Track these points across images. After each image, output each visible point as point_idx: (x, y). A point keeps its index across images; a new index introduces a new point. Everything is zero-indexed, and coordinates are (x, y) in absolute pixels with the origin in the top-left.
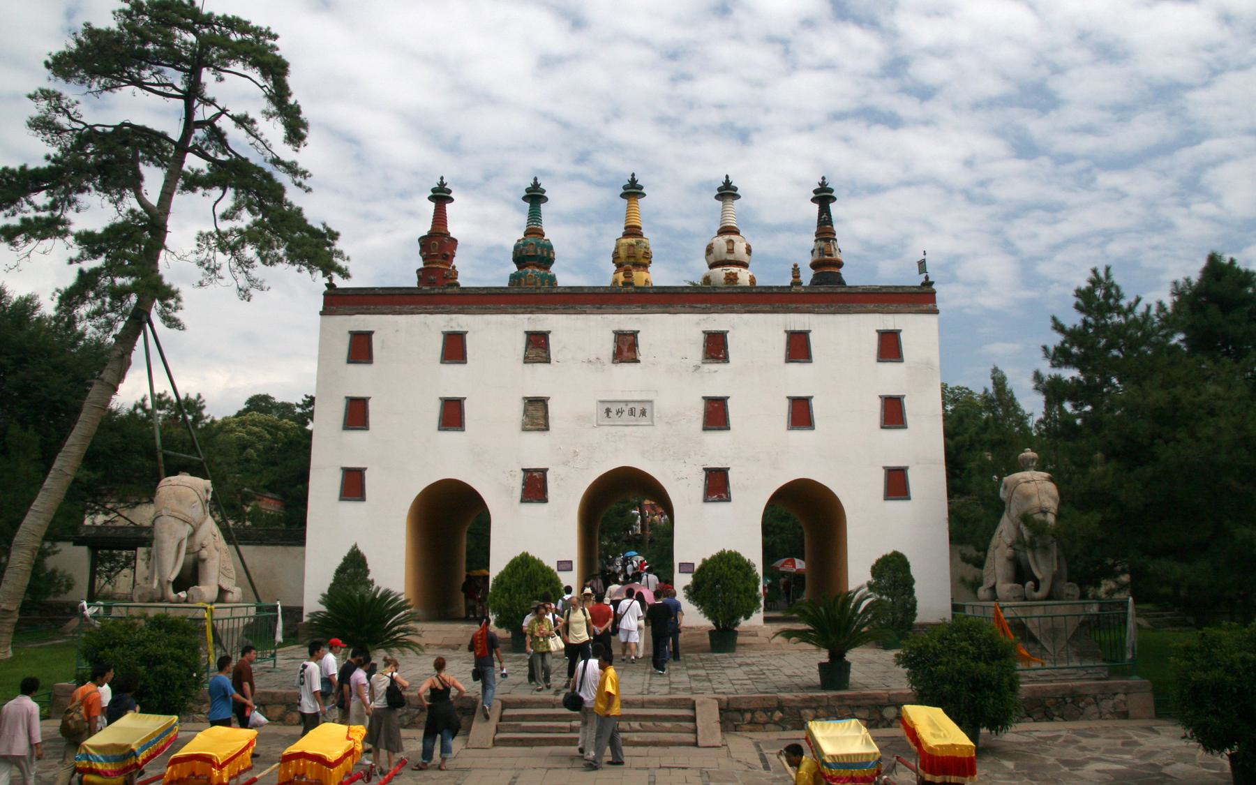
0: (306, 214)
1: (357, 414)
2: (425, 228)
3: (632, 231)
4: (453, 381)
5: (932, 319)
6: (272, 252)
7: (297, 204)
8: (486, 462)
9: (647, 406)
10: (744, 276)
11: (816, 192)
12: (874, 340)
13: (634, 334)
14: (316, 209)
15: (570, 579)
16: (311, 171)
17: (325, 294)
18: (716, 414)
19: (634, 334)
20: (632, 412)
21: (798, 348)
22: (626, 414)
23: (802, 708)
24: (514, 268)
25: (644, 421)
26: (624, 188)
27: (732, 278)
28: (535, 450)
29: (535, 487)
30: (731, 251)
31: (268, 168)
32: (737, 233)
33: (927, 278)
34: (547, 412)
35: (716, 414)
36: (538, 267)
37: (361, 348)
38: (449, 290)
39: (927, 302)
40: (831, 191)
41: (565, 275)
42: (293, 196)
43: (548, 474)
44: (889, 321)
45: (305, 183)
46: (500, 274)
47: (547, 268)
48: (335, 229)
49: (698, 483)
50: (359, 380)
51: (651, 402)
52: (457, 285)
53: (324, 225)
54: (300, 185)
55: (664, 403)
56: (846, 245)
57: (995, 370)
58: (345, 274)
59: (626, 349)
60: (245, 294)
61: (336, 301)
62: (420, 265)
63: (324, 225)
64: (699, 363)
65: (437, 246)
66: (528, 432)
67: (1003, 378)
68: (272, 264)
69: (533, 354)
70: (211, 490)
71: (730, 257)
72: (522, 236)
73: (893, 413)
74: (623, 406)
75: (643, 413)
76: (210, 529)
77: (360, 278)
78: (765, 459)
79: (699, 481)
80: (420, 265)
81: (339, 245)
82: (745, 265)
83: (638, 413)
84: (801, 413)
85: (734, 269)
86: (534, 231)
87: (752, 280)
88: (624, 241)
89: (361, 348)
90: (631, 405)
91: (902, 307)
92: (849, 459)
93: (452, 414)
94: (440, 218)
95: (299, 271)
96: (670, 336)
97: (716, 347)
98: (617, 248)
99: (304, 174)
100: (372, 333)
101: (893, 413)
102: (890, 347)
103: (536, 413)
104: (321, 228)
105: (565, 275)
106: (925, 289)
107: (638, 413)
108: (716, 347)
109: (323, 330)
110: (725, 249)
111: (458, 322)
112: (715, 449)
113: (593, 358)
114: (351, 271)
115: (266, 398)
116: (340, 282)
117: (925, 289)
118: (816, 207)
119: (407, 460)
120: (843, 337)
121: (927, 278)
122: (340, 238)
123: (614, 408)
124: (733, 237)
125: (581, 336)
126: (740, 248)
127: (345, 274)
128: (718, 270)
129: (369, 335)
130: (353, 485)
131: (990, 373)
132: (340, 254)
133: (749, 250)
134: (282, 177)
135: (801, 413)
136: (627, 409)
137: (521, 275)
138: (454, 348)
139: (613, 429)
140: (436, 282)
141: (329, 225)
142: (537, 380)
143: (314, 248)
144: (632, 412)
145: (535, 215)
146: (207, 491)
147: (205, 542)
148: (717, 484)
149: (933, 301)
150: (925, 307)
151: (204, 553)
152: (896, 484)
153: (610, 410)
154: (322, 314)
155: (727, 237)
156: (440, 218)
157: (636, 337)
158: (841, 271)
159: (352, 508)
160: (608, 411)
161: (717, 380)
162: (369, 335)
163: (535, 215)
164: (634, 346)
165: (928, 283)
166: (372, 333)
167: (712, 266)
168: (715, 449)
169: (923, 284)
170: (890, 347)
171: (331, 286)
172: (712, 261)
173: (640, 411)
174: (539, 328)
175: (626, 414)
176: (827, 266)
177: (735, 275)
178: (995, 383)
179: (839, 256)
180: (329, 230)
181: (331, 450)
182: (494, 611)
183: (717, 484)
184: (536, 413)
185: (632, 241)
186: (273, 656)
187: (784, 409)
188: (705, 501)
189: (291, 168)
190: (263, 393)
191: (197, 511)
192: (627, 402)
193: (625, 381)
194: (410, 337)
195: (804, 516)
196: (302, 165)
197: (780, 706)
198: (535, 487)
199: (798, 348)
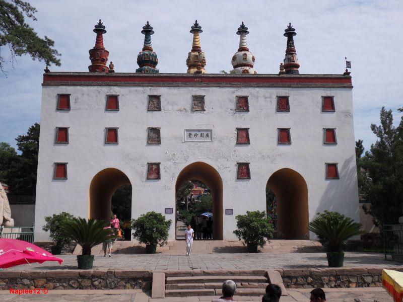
1: (62, 136)
2: (92, 45)
3: (196, 49)
4: (112, 120)
9: (209, 133)
12: (320, 100)
15: (171, 217)
17: (44, 75)
20: (202, 135)
23: (322, 276)
24: (138, 67)
25: (208, 140)
26: (286, 30)
28: (154, 154)
29: (154, 171)
32: (248, 50)
35: (243, 136)
36: (150, 66)
37: (64, 103)
40: (294, 30)
43: (161, 165)
44: (328, 93)
47: (154, 67)
50: (64, 119)
51: (211, 131)
55: (217, 132)
56: (299, 58)
58: (58, 63)
61: (50, 79)
62: (90, 64)
63: (46, 37)
65: (98, 54)
66: (151, 147)
71: (244, 62)
72: (142, 51)
77: (64, 68)
78: (267, 159)
79: (234, 169)
80: (90, 64)
82: (252, 66)
83: (205, 135)
85: (247, 68)
86: (147, 48)
88: (193, 54)
89: (64, 103)
93: (112, 136)
94: (99, 40)
96: (220, 98)
98: (189, 57)
103: (154, 136)
104: (44, 39)
107: (205, 135)
109: (43, 93)
111: (115, 90)
112: (243, 153)
113: (182, 109)
116: (53, 68)
118: (286, 38)
119: (87, 159)
120: (305, 101)
123: (193, 133)
124: (246, 52)
126: (250, 57)
127: (58, 63)
128: (239, 68)
130: (61, 171)
132: (55, 51)
133: (254, 59)
139: (192, 144)
140: (99, 71)
141: (49, 37)
142: (154, 120)
143: (42, 49)
144: (202, 135)
145: (147, 40)
148: (244, 171)
149: (350, 82)
150: (345, 85)
153: (190, 133)
154: (43, 85)
155: (243, 52)
156: (99, 40)
157: (204, 98)
158: (299, 69)
159: (59, 184)
160: (190, 135)
161: (243, 120)
163: (147, 40)
167: (235, 67)
168: (243, 153)
169: (345, 74)
171: (47, 71)
172: (235, 64)
173: (207, 134)
174: (155, 93)
175: (199, 136)
176: (290, 66)
179: (297, 62)
180: (48, 40)
181: (48, 154)
182: (42, 253)
183: (244, 171)
184: (154, 136)
185: (197, 53)
187: (275, 134)
192: (199, 131)
193: (198, 120)
194: (89, 98)
195: (286, 188)
197: (311, 274)
198: (154, 171)
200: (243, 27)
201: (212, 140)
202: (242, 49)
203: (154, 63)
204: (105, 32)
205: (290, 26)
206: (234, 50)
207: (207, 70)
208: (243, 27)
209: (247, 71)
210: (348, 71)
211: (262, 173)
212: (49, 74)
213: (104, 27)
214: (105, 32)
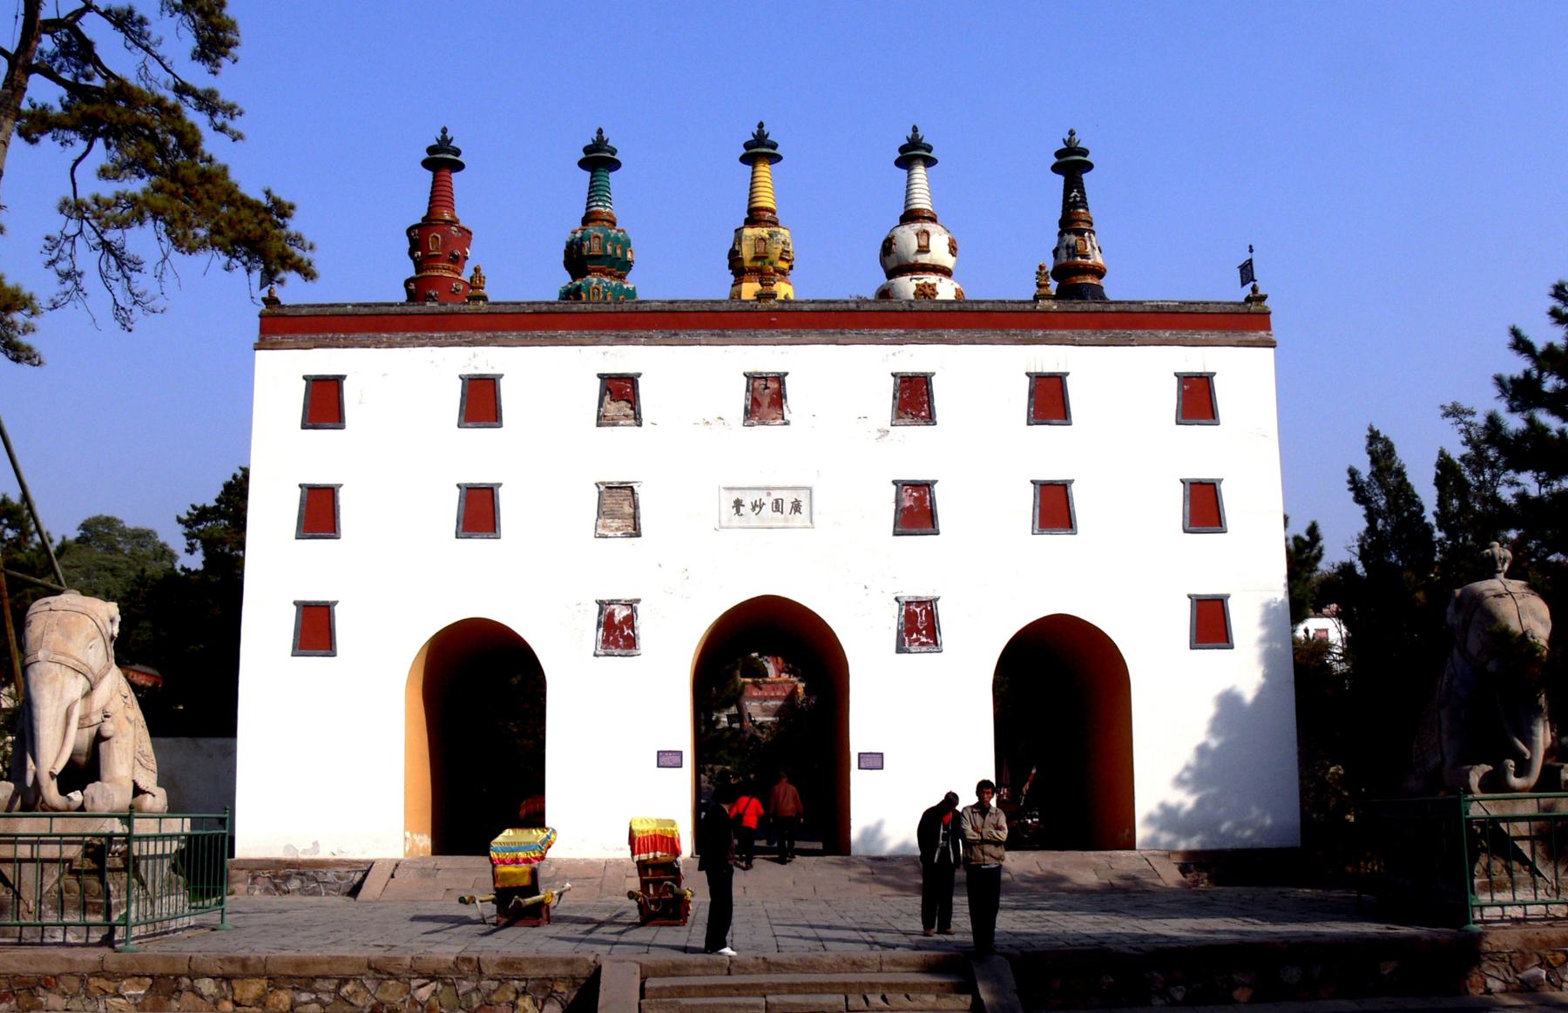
0: (234, 176)
2: (417, 213)
5: (1269, 353)
6: (190, 233)
7: (221, 159)
8: (535, 589)
10: (946, 290)
11: (1059, 154)
13: (780, 378)
14: (247, 166)
16: (241, 106)
18: (917, 511)
19: (780, 378)
20: (778, 506)
21: (1049, 400)
22: (767, 509)
25: (799, 519)
26: (747, 146)
27: (926, 292)
28: (618, 569)
30: (924, 249)
31: (171, 98)
33: (1254, 289)
34: (636, 507)
35: (917, 511)
36: (609, 274)
38: (472, 307)
39: (1255, 329)
40: (1085, 152)
41: (649, 283)
42: (214, 145)
44: (1195, 359)
45: (231, 125)
46: (546, 282)
47: (621, 277)
48: (286, 198)
49: (889, 621)
52: (484, 298)
53: (268, 193)
54: (221, 129)
57: (1374, 437)
59: (766, 398)
60: (122, 317)
63: (268, 193)
64: (887, 426)
67: (1389, 449)
68: (191, 250)
69: (612, 408)
70: (118, 619)
71: (924, 259)
73: (1204, 507)
74: (762, 495)
75: (796, 507)
76: (115, 690)
78: (997, 586)
81: (293, 225)
82: (946, 272)
83: (787, 507)
84: (1055, 507)
85: (931, 279)
87: (959, 293)
88: (748, 232)
90: (776, 495)
91: (1215, 335)
92: (1127, 584)
93: (479, 511)
94: (440, 196)
95: (228, 268)
96: (842, 380)
97: (914, 398)
99: (230, 110)
100: (343, 377)
101: (1204, 507)
102: (1197, 401)
103: (619, 506)
104: (263, 200)
105: (649, 283)
106: (1253, 307)
107: (787, 507)
108: (914, 398)
110: (915, 247)
112: (918, 566)
114: (317, 267)
115: (109, 522)
117: (1253, 307)
118: (1060, 180)
120: (1124, 383)
121: (1254, 289)
122: (295, 214)
123: (748, 501)
124: (929, 226)
125: (692, 380)
129: (336, 382)
130: (315, 629)
131: (1365, 442)
134: (193, 115)
135: (1055, 507)
136: (769, 501)
137: (579, 288)
138: (481, 402)
141: (276, 194)
144: (778, 506)
145: (596, 191)
146: (112, 621)
147: (110, 709)
150: (1252, 336)
151: (108, 729)
152: (1210, 623)
155: (917, 226)
156: (440, 196)
158: (1103, 282)
160: (738, 504)
162: (336, 382)
164: (779, 399)
165: (1257, 298)
166: (343, 377)
167: (891, 274)
169: (1248, 300)
170: (1197, 401)
172: (892, 264)
173: (793, 505)
175: (767, 509)
177: (932, 287)
178: (1374, 461)
180: (277, 203)
185: (763, 232)
186: (221, 903)
188: (900, 649)
189: (208, 102)
190: (107, 513)
191: (97, 654)
193: (767, 454)
196: (225, 96)
199: (1049, 400)
206: (571, 223)
212: (277, 311)
213: (929, 149)
214: (459, 166)
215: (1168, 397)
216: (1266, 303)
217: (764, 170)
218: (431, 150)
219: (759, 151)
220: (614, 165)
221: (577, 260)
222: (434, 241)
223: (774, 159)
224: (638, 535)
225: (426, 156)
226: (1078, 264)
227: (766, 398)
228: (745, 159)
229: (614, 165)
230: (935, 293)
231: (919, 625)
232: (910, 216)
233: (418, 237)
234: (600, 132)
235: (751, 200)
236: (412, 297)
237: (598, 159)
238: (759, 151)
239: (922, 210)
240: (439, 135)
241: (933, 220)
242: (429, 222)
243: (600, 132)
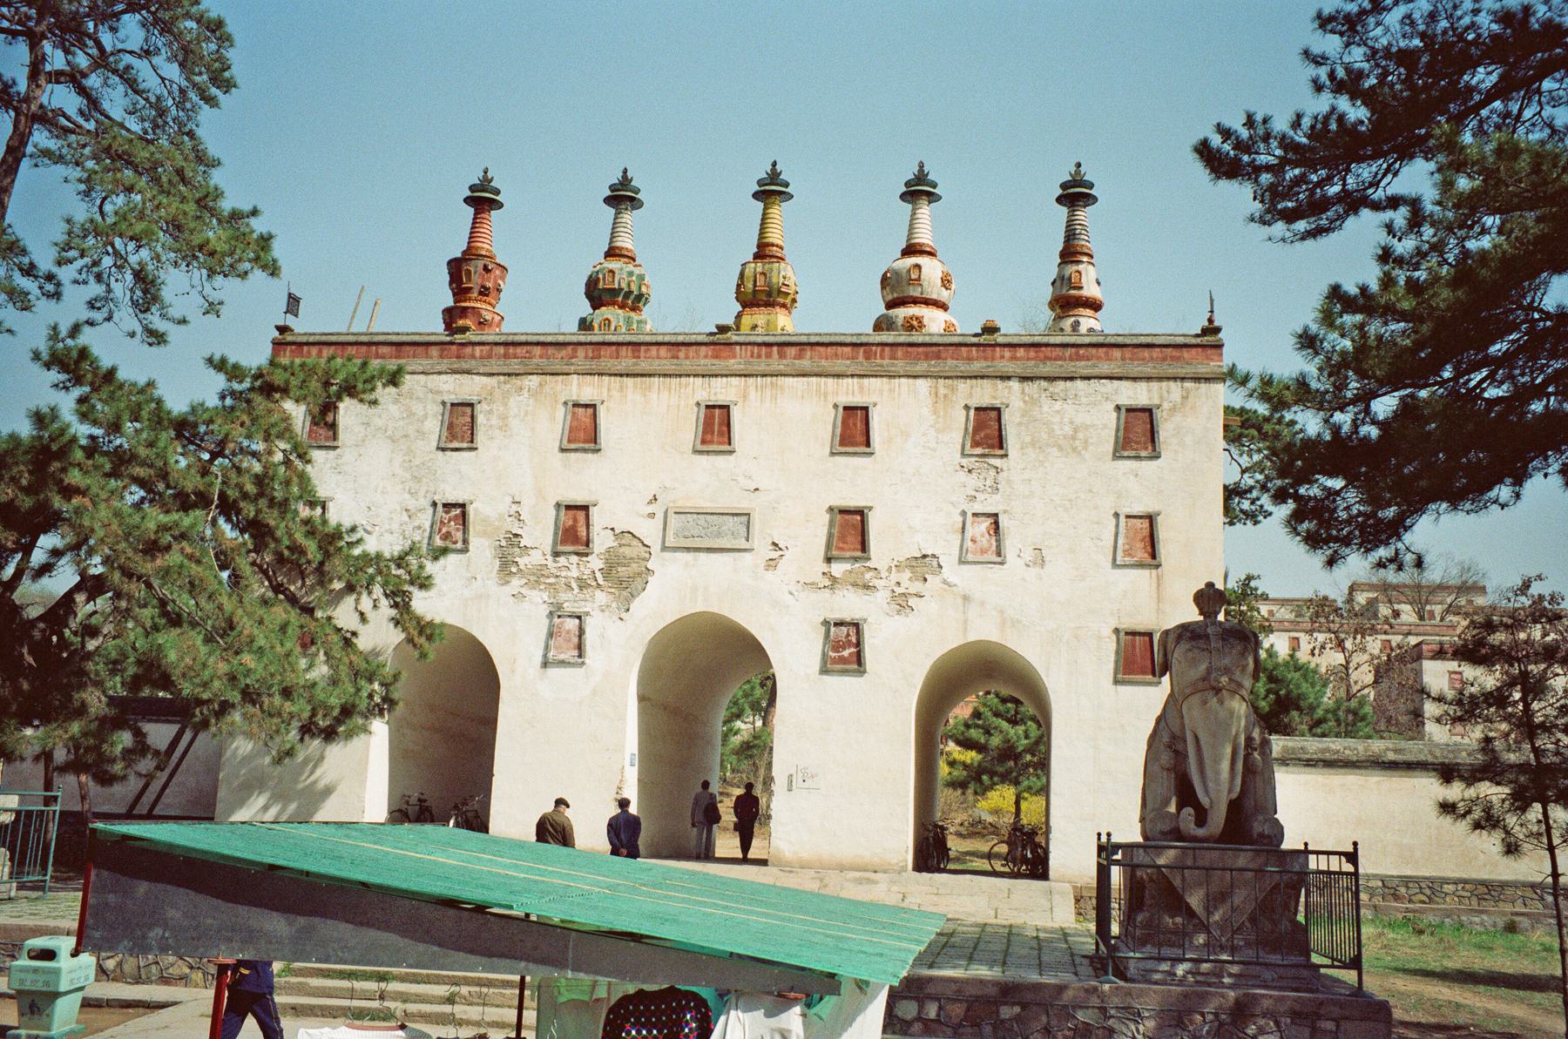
26: (760, 183)
27: (912, 325)
44: (851, 392)
46: (563, 311)
103: (851, 529)
167: (891, 305)
169: (1205, 332)
183: (846, 649)
200: (774, 176)
201: (999, 554)
202: (764, 252)
203: (634, 300)
204: (499, 205)
205: (1078, 172)
206: (591, 258)
207: (656, 320)
208: (774, 176)
209: (919, 319)
210: (1216, 324)
211: (906, 653)
212: (289, 338)
213: (637, 191)
214: (499, 205)
215: (825, 423)
216: (1220, 335)
217: (925, 211)
218: (472, 188)
219: (918, 191)
220: (635, 203)
221: (598, 294)
222: (468, 276)
223: (932, 197)
224: (961, 562)
225: (609, 193)
226: (1071, 296)
227: (716, 427)
228: (609, 201)
229: (1089, 199)
230: (921, 325)
231: (846, 649)
232: (911, 250)
233: (457, 269)
234: (921, 165)
235: (611, 242)
236: (449, 326)
237: (622, 197)
238: (918, 191)
239: (621, 249)
240: (620, 175)
241: (932, 254)
242: (470, 254)
243: (921, 165)
